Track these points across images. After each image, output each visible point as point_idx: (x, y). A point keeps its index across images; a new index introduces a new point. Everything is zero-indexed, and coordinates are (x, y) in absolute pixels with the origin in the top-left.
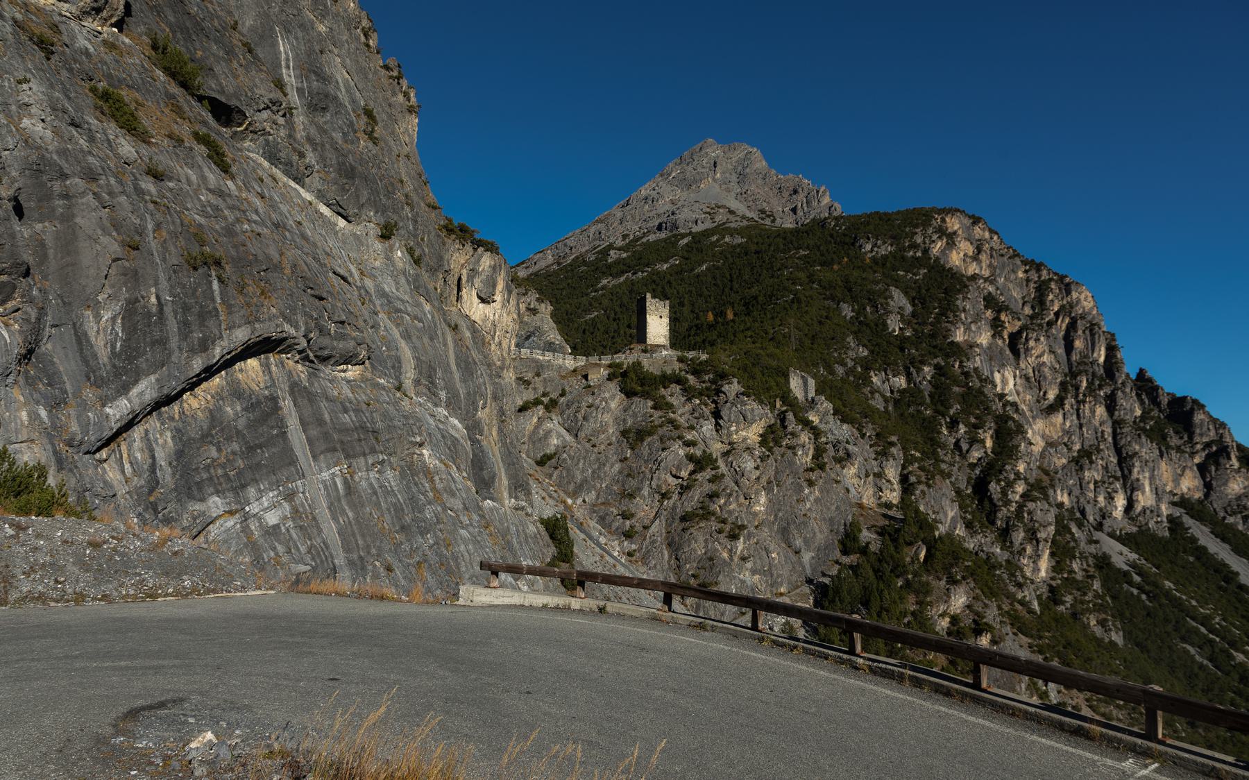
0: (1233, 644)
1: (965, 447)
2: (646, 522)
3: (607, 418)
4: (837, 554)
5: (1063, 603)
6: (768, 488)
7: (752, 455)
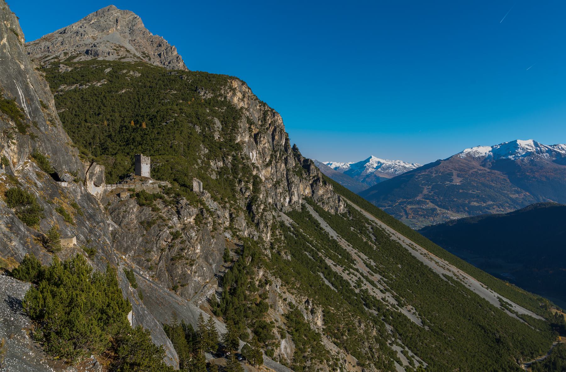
0: (318, 250)
1: (244, 191)
2: (157, 262)
3: (133, 216)
4: (223, 263)
5: (275, 248)
6: (200, 243)
7: (193, 229)
